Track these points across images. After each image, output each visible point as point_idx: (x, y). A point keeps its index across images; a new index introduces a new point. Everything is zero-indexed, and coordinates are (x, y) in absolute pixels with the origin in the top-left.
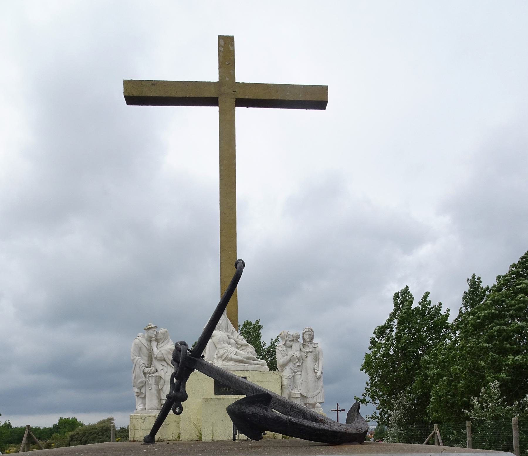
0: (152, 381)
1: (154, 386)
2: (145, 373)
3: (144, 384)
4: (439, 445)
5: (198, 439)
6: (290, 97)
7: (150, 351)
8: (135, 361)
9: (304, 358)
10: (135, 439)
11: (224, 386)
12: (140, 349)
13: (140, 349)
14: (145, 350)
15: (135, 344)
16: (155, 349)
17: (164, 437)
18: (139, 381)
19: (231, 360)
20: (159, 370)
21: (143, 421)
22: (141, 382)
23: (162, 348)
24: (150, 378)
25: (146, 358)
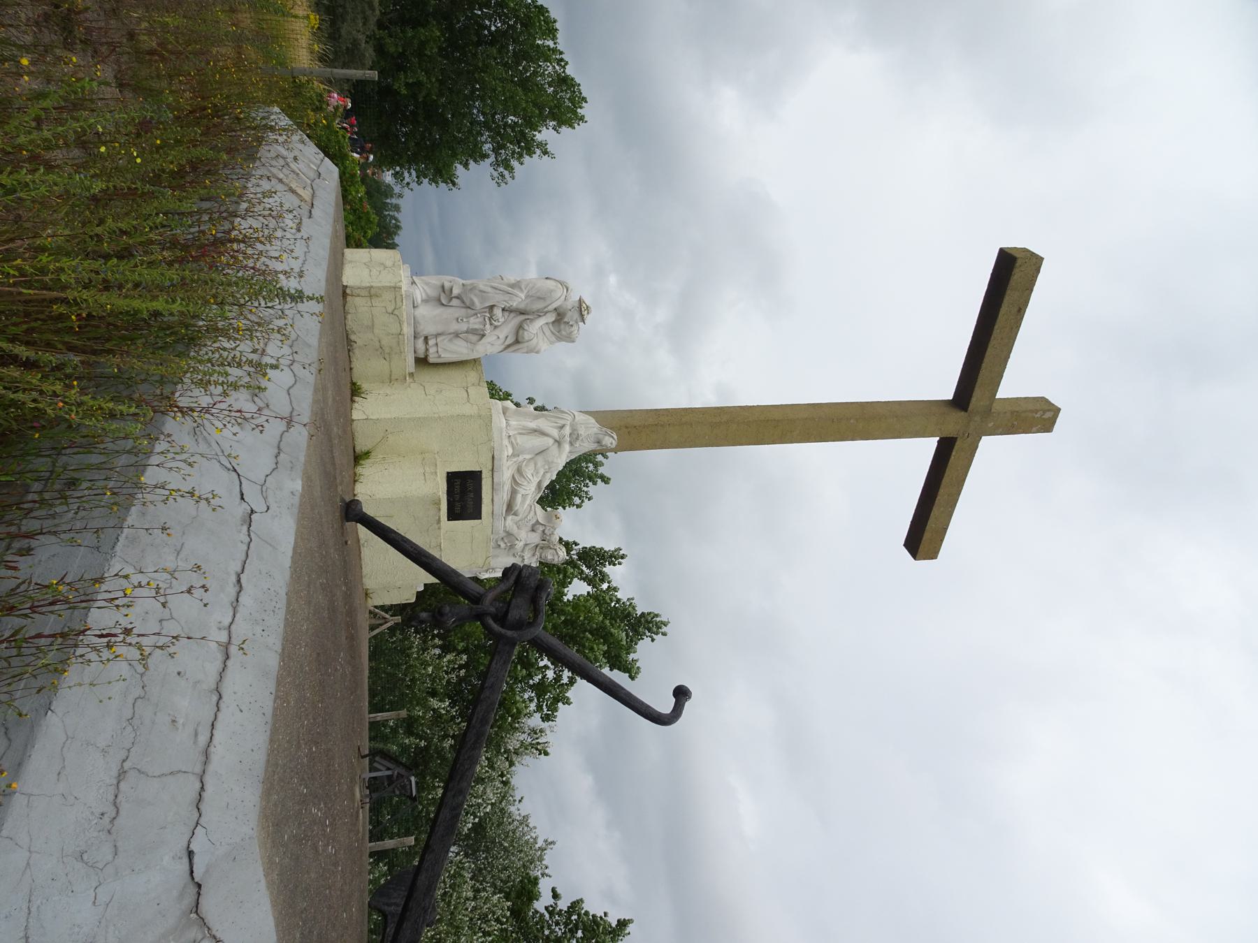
0: (475, 323)
1: (464, 327)
2: (492, 307)
3: (469, 307)
4: (372, 628)
5: (358, 449)
6: (935, 512)
7: (539, 314)
8: (516, 291)
9: (512, 551)
10: (349, 298)
11: (464, 491)
12: (544, 299)
13: (544, 299)
14: (539, 305)
15: (552, 291)
16: (541, 322)
17: (356, 351)
18: (476, 300)
19: (514, 493)
20: (497, 332)
21: (390, 310)
22: (473, 303)
23: (540, 335)
24: (481, 319)
25: (522, 306)
